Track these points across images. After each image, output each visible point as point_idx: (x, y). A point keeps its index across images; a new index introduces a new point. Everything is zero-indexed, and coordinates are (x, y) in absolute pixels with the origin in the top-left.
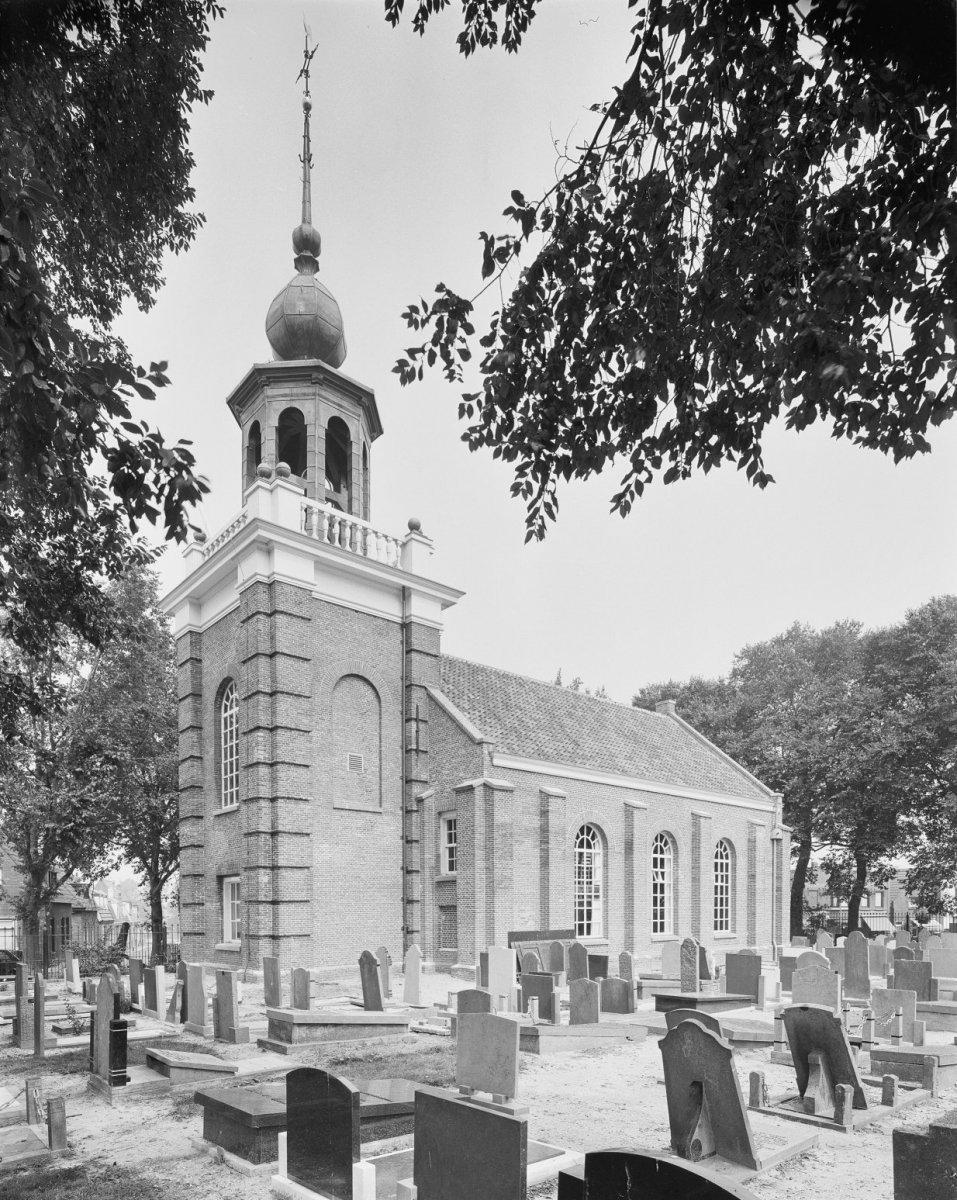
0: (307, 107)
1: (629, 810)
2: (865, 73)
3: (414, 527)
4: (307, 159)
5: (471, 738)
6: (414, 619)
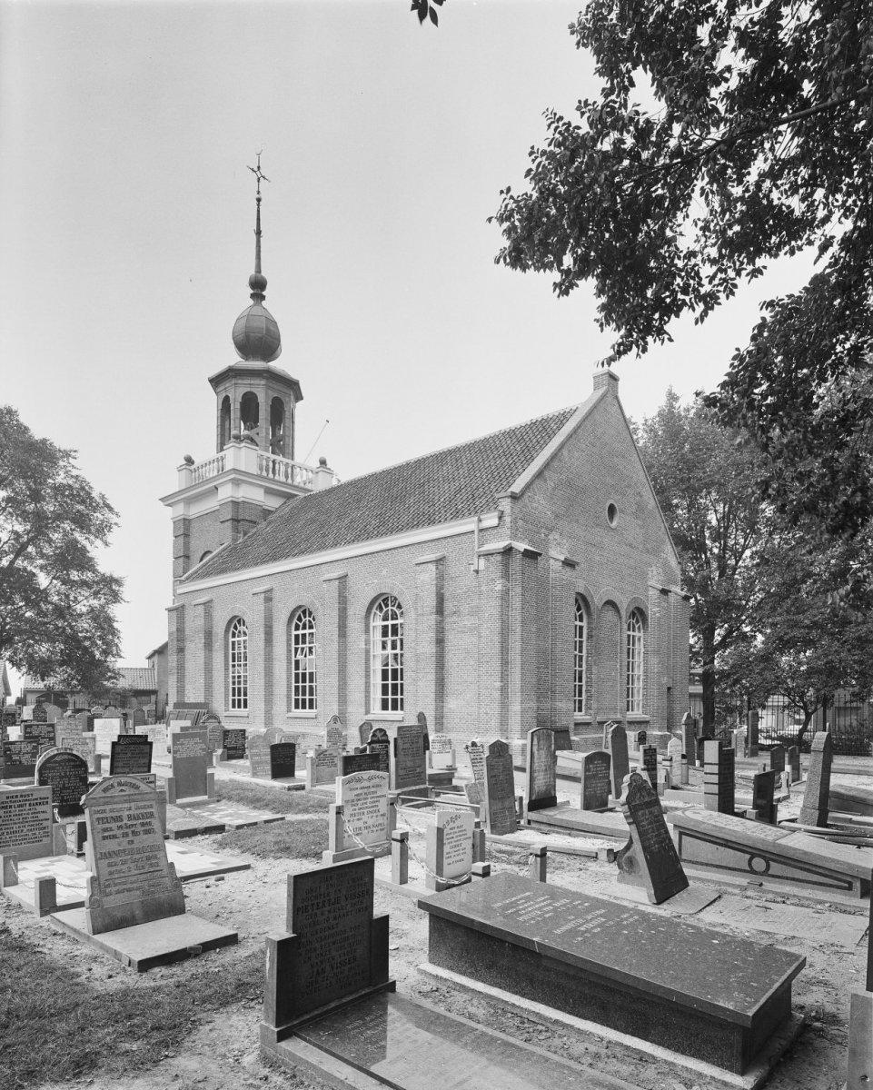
0: (259, 200)
1: (268, 597)
2: (653, 314)
3: (323, 462)
4: (258, 233)
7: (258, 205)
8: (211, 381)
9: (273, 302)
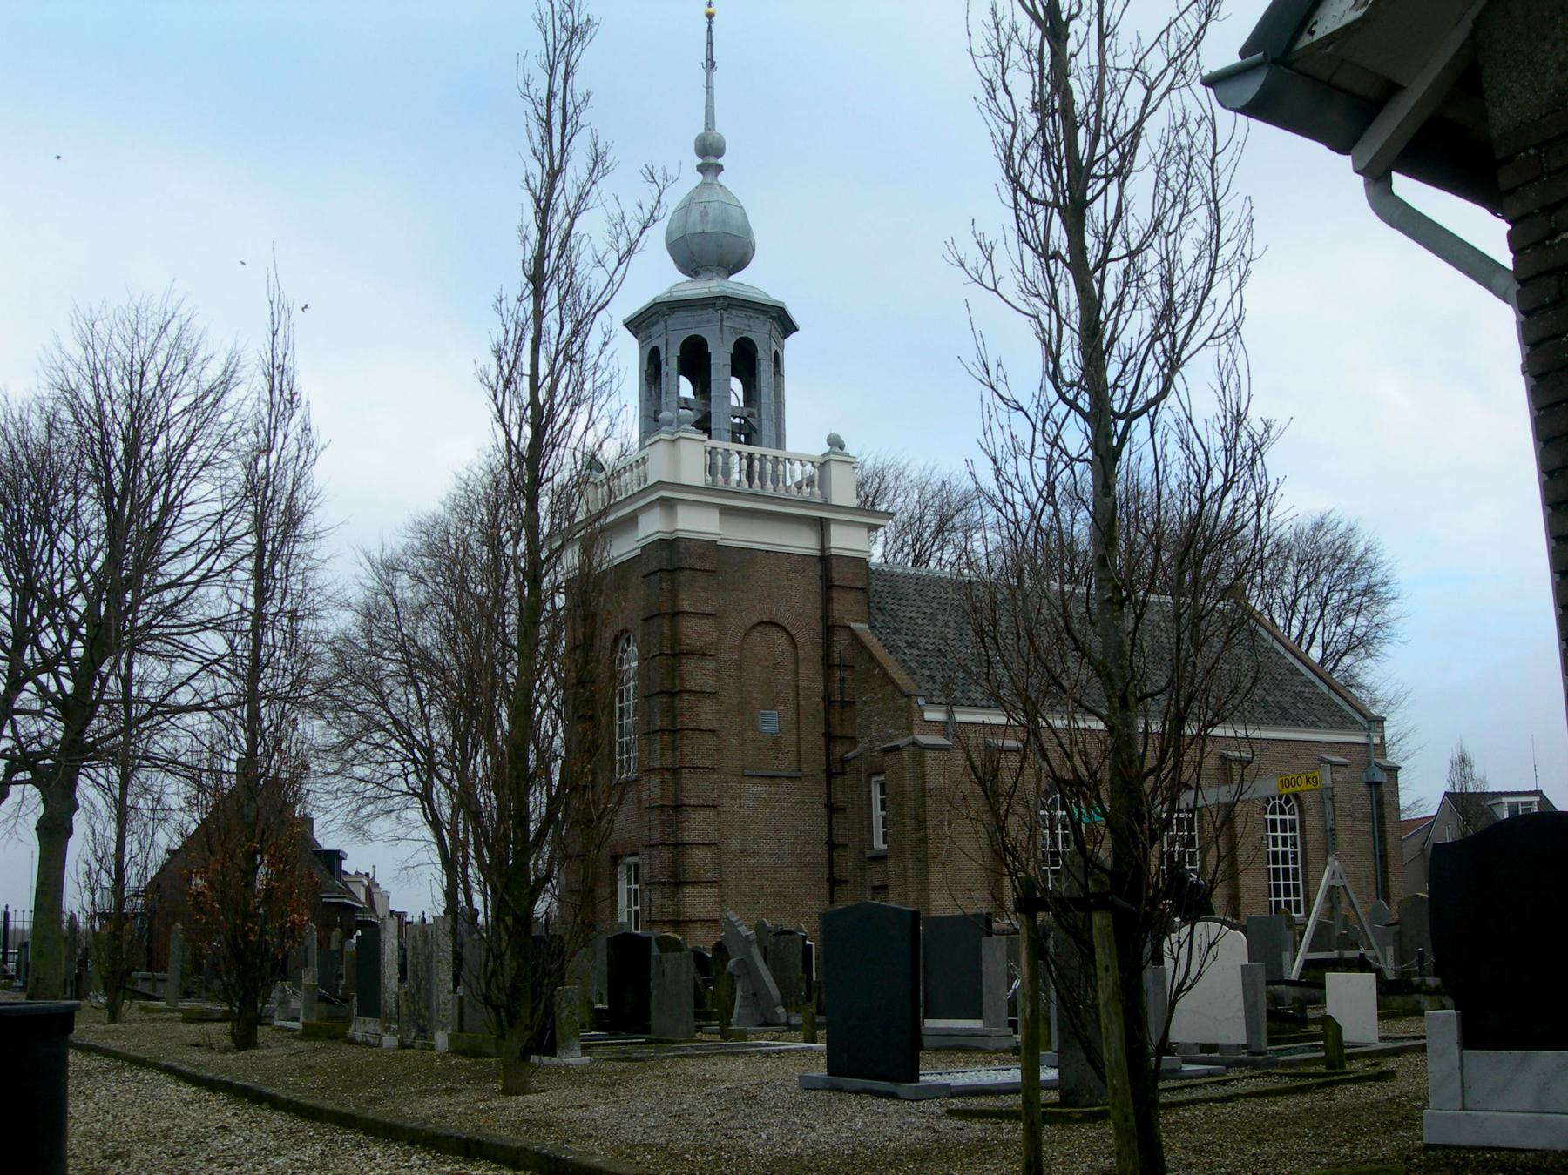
0: (710, 16)
5: (897, 687)
6: (834, 552)
7: (710, 23)
8: (627, 325)
9: (738, 176)
